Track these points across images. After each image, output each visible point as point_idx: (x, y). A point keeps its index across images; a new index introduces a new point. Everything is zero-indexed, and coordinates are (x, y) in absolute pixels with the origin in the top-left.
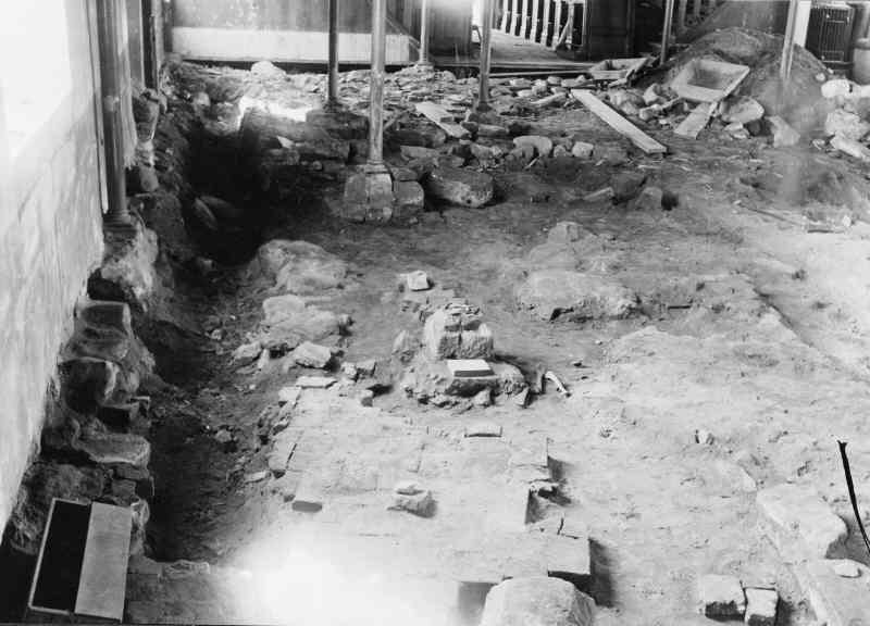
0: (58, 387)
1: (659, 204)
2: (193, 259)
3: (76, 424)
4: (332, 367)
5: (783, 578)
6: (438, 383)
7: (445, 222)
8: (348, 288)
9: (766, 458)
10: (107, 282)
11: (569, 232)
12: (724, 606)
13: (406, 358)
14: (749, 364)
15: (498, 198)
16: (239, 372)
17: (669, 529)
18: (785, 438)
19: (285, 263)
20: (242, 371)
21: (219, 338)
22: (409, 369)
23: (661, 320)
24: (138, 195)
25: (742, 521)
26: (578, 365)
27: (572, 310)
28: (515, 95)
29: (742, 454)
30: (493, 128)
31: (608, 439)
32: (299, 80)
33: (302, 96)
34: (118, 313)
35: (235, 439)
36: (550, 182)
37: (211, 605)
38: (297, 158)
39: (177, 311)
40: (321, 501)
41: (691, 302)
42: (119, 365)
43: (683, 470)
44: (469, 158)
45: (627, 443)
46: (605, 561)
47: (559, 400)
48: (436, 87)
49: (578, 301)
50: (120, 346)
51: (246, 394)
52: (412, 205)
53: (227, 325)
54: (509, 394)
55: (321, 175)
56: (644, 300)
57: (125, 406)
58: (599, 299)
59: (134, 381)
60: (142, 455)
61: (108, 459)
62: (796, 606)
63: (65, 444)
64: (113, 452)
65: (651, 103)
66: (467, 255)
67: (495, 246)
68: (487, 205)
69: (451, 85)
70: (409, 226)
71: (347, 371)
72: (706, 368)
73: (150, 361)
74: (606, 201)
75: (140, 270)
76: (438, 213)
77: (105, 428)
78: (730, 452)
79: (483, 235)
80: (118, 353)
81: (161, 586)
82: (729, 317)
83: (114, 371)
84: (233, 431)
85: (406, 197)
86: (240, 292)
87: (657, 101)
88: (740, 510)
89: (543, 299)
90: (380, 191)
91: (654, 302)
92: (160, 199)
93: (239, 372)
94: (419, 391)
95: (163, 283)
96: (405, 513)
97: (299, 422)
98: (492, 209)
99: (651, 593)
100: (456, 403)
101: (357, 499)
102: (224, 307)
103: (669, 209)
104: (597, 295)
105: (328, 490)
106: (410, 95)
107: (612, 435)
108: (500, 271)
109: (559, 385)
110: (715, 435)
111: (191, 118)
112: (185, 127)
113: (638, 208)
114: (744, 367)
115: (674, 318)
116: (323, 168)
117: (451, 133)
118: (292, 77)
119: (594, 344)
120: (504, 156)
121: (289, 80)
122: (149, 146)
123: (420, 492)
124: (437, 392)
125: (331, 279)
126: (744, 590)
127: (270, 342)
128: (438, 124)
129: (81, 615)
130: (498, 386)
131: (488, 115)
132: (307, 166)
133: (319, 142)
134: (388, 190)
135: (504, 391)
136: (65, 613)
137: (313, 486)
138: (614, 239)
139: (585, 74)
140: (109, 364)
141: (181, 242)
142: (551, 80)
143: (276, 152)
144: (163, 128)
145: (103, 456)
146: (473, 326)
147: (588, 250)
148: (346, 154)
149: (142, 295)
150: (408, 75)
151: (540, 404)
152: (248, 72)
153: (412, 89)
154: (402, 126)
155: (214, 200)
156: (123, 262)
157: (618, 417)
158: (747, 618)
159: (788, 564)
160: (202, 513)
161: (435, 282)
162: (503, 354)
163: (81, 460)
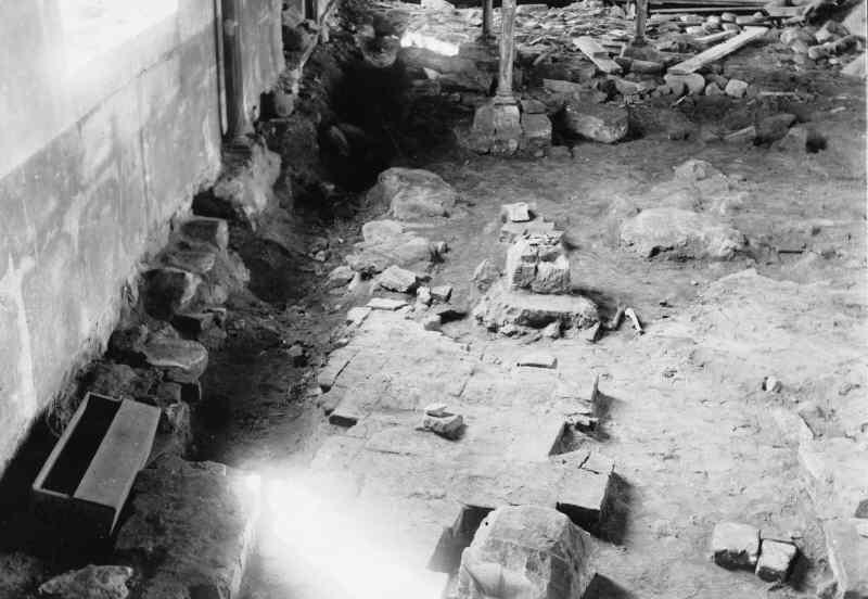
0: (135, 293)
1: (803, 146)
2: (317, 183)
3: (145, 330)
4: (412, 292)
5: (811, 534)
6: (509, 312)
7: (573, 156)
8: (454, 217)
9: (833, 411)
10: (219, 200)
11: (695, 171)
12: (735, 555)
13: (484, 285)
14: (845, 313)
15: (635, 133)
16: (331, 292)
17: (706, 474)
18: (856, 390)
19: (399, 190)
20: (336, 291)
21: (323, 259)
22: (484, 297)
23: (769, 264)
24: (273, 120)
25: (786, 473)
26: (664, 304)
27: (672, 249)
28: (683, 31)
29: (807, 406)
30: (648, 64)
31: (672, 379)
32: (465, 14)
33: (465, 30)
34: (213, 227)
35: (307, 354)
36: (696, 120)
37: (212, 504)
38: (438, 89)
39: (289, 232)
40: (356, 417)
41: (805, 247)
42: (203, 277)
43: (741, 417)
44: (612, 92)
45: (694, 385)
46: (627, 499)
47: (631, 337)
48: (602, 22)
49: (680, 240)
50: (206, 260)
51: (331, 313)
52: (540, 138)
53: (333, 247)
54: (579, 327)
55: (459, 106)
56: (752, 242)
57: (199, 315)
58: (703, 239)
59: (220, 294)
60: (197, 361)
61: (163, 362)
62: (816, 564)
63: (128, 346)
64: (170, 357)
65: (823, 42)
66: (585, 190)
67: (617, 182)
68: (620, 141)
69: (618, 21)
70: (535, 159)
71: (421, 296)
72: (797, 315)
73: (243, 275)
74: (747, 142)
75: (256, 190)
76: (567, 148)
77: (177, 335)
78: (797, 402)
79: (608, 171)
80: (203, 266)
81: (172, 482)
82: (838, 265)
83: (193, 283)
84: (306, 348)
85: (534, 130)
86: (357, 218)
87: (830, 40)
88: (788, 461)
89: (645, 236)
90: (508, 123)
91: (764, 245)
92: (293, 124)
93: (331, 292)
94: (489, 319)
95: (281, 204)
96: (432, 435)
97: (359, 341)
98: (625, 145)
99: (666, 535)
100: (525, 334)
101: (393, 418)
102: (338, 231)
103: (816, 152)
104: (702, 235)
105: (368, 408)
106: (572, 30)
107: (676, 376)
108: (611, 206)
109: (636, 322)
110: (784, 383)
111: (352, 49)
112: (342, 58)
113: (781, 150)
114: (840, 316)
115: (783, 263)
116: (461, 99)
117: (602, 68)
118: (461, 11)
119: (690, 285)
120: (650, 92)
121: (457, 14)
122: (297, 74)
123: (452, 415)
124: (506, 322)
125: (438, 207)
126: (761, 541)
127: (360, 264)
128: (591, 58)
129: (80, 500)
130: (569, 319)
131: (644, 50)
132: (446, 97)
133: (463, 74)
134: (515, 122)
135: (575, 325)
136: (65, 496)
137: (354, 403)
138: (745, 180)
139: (761, 11)
140: (189, 276)
141: (310, 166)
142: (725, 17)
143: (419, 82)
144: (320, 56)
145: (158, 359)
146: (549, 258)
147: (712, 190)
148: (487, 87)
149: (252, 214)
150: (577, 10)
151: (612, 342)
152: (418, 6)
153: (577, 24)
154: (555, 60)
155: (351, 128)
156: (235, 182)
157: (686, 358)
158: (758, 569)
159: (819, 520)
160: (257, 422)
161: (536, 213)
162: (590, 288)
163: (138, 361)
